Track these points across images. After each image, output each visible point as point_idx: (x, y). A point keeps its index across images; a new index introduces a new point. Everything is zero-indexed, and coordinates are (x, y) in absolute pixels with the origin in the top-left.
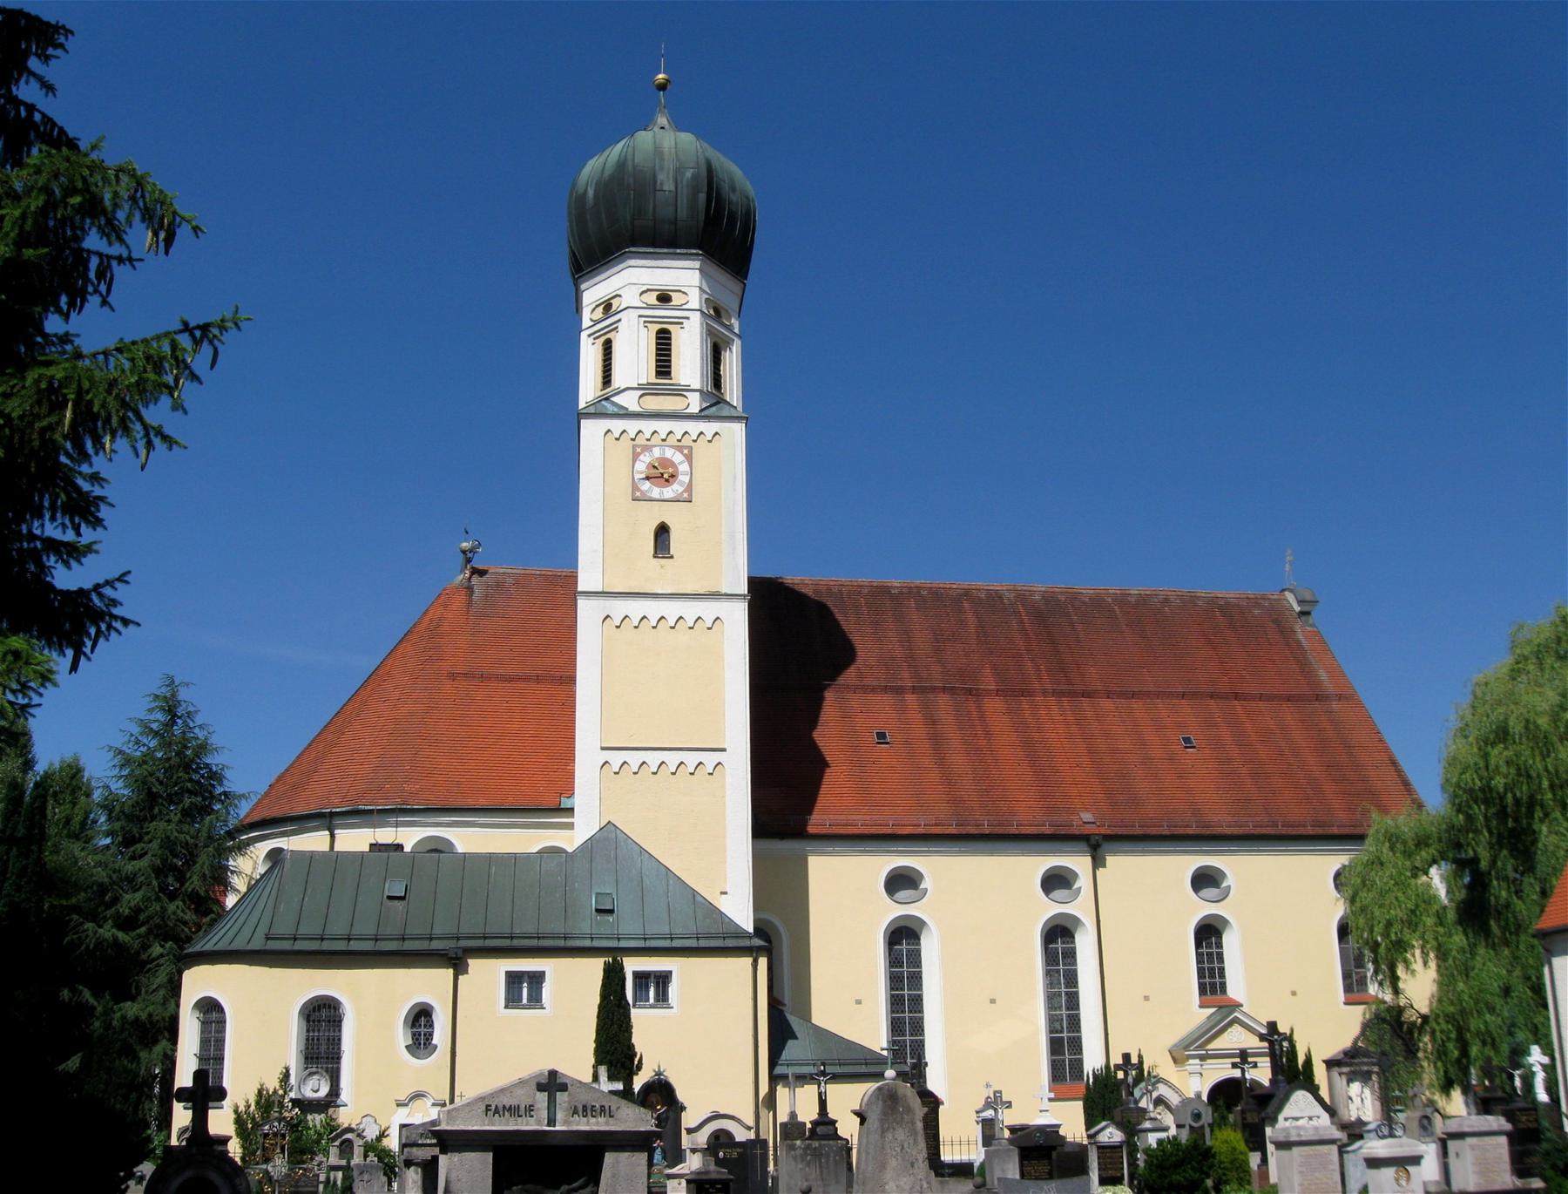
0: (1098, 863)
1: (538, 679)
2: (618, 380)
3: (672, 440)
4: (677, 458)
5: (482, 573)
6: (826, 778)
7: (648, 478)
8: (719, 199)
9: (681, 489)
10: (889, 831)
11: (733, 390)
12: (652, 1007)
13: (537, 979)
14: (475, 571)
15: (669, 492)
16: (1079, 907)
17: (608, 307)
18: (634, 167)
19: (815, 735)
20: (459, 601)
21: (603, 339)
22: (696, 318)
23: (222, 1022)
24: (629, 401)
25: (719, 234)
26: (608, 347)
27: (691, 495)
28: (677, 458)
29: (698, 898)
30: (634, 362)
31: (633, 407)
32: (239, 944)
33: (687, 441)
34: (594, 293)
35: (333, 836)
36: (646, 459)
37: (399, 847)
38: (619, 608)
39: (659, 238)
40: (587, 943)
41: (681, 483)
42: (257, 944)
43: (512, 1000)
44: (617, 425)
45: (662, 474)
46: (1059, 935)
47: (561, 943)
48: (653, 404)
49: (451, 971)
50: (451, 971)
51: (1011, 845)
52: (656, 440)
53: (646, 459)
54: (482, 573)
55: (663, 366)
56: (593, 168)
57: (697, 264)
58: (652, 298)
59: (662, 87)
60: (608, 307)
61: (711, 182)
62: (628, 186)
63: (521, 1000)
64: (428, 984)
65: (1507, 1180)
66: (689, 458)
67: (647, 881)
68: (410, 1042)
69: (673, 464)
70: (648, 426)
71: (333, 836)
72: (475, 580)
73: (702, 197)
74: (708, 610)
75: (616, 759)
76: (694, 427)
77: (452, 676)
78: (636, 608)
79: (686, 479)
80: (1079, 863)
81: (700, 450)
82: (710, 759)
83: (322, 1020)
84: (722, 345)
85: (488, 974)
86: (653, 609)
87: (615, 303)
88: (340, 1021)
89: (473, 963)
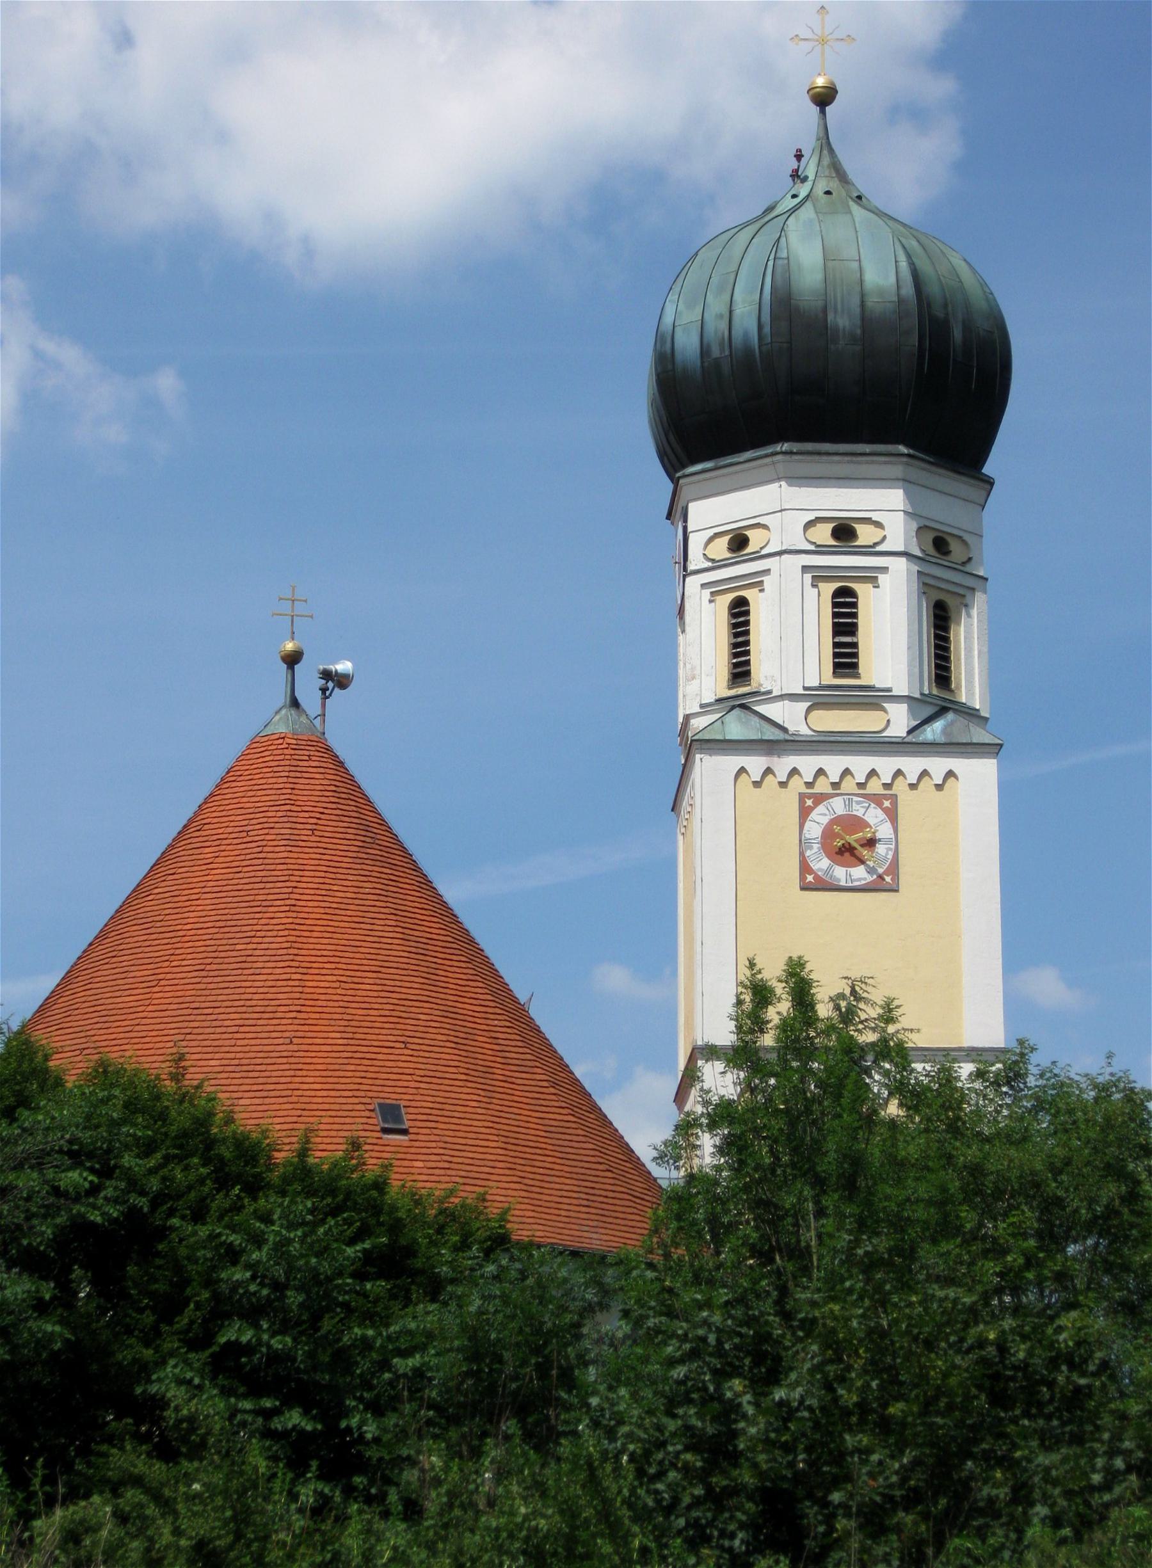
3: (848, 785)
4: (874, 816)
11: (972, 685)
21: (730, 597)
24: (792, 717)
26: (740, 610)
30: (791, 646)
33: (874, 787)
36: (820, 818)
53: (820, 818)
55: (846, 659)
60: (739, 542)
65: (829, 679)
66: (892, 815)
84: (951, 602)
87: (756, 539)
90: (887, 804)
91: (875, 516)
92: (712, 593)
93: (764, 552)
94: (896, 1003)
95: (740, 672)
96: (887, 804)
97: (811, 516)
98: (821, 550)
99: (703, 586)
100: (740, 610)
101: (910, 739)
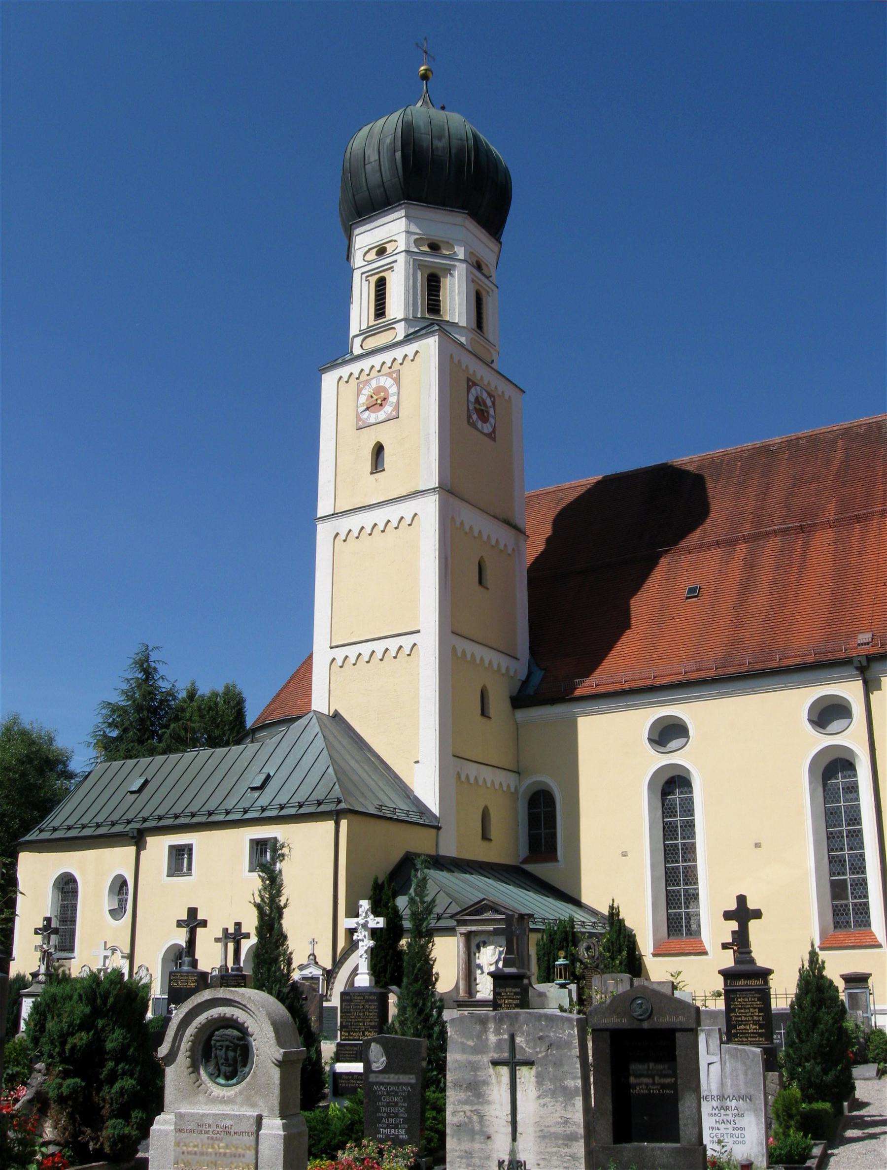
0: (870, 686)
3: (385, 369)
6: (624, 639)
10: (649, 682)
16: (851, 737)
19: (632, 601)
21: (377, 276)
23: (75, 892)
34: (366, 238)
36: (367, 391)
46: (834, 770)
49: (133, 849)
50: (133, 849)
51: (776, 679)
52: (374, 373)
55: (380, 310)
57: (402, 213)
59: (425, 77)
64: (117, 860)
66: (397, 381)
73: (399, 154)
74: (405, 509)
75: (339, 654)
80: (850, 690)
82: (406, 642)
83: (67, 887)
85: (158, 847)
89: (151, 841)
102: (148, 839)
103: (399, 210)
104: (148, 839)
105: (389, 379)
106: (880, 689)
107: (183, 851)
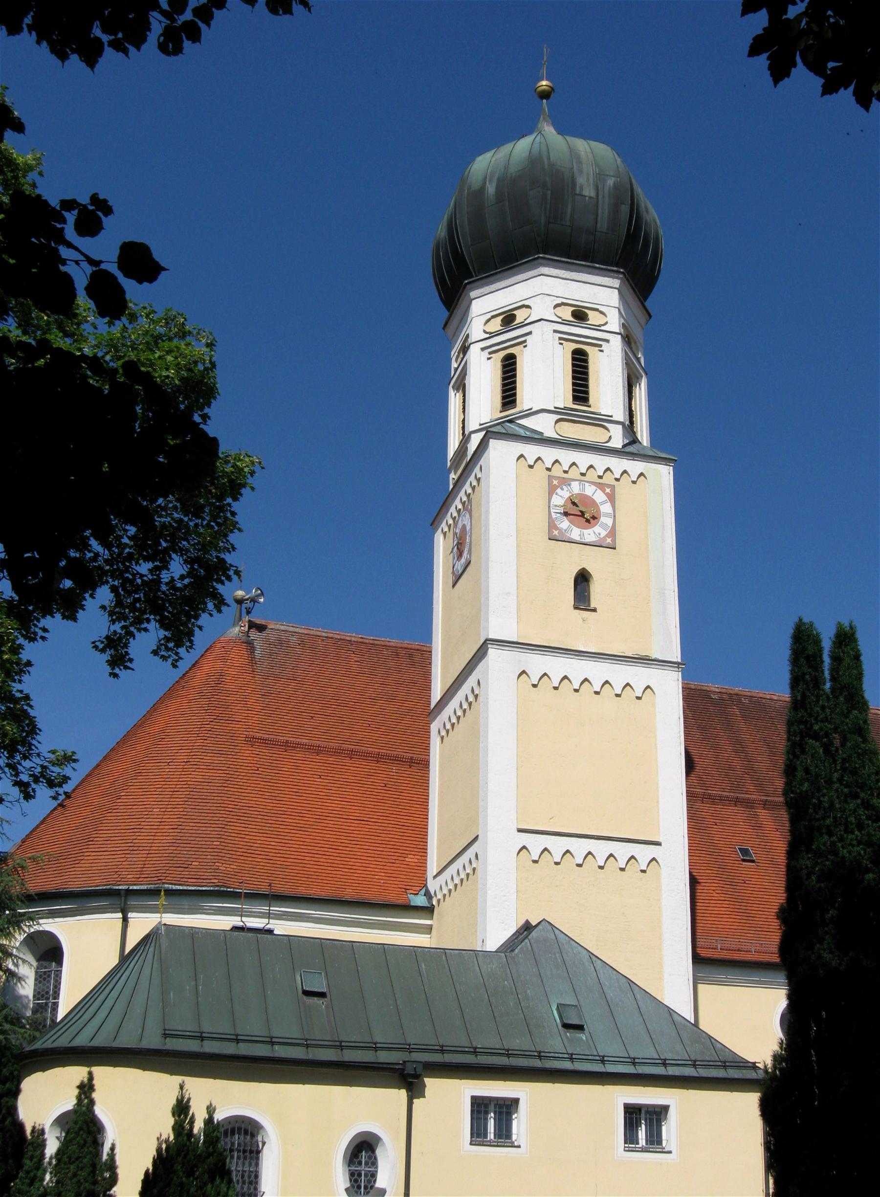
1: (352, 754)
2: (526, 398)
3: (592, 476)
4: (599, 497)
5: (261, 628)
7: (566, 514)
8: (639, 217)
9: (604, 533)
12: (643, 1150)
13: (506, 1109)
14: (252, 625)
15: (591, 534)
17: (509, 319)
18: (551, 165)
20: (238, 657)
21: (502, 354)
22: (616, 345)
24: (545, 425)
25: (632, 258)
26: (509, 366)
27: (614, 540)
28: (599, 497)
29: (675, 1017)
30: (544, 380)
31: (549, 432)
32: (126, 1040)
33: (608, 479)
34: (485, 304)
35: (125, 920)
37: (270, 932)
38: (537, 664)
39: (575, 249)
40: (567, 1065)
41: (604, 526)
42: (153, 1041)
43: (478, 1134)
44: (532, 451)
45: (581, 512)
47: (537, 1063)
48: (571, 431)
52: (574, 473)
54: (261, 628)
56: (485, 165)
57: (616, 283)
58: (566, 313)
59: (545, 95)
60: (509, 319)
61: (626, 200)
62: (547, 183)
63: (485, 1136)
64: (372, 1107)
66: (611, 498)
67: (610, 994)
68: (348, 1185)
69: (594, 503)
70: (566, 456)
71: (125, 920)
72: (254, 634)
73: (625, 209)
74: (639, 676)
75: (536, 843)
76: (618, 464)
77: (251, 741)
78: (557, 666)
79: (609, 522)
81: (623, 489)
82: (644, 853)
85: (449, 1098)
86: (577, 669)
87: (520, 316)
88: (258, 1152)
89: (432, 1084)
90: (608, 490)
91: (601, 308)
92: (490, 353)
93: (526, 322)
94: (23, 983)
95: (509, 396)
96: (608, 490)
97: (559, 301)
98: (564, 322)
99: (483, 349)
100: (509, 366)
101: (628, 449)
102: (428, 1081)
103: (613, 278)
104: (428, 1081)
105: (559, 491)
106: (424, 1097)
107: (486, 1106)
